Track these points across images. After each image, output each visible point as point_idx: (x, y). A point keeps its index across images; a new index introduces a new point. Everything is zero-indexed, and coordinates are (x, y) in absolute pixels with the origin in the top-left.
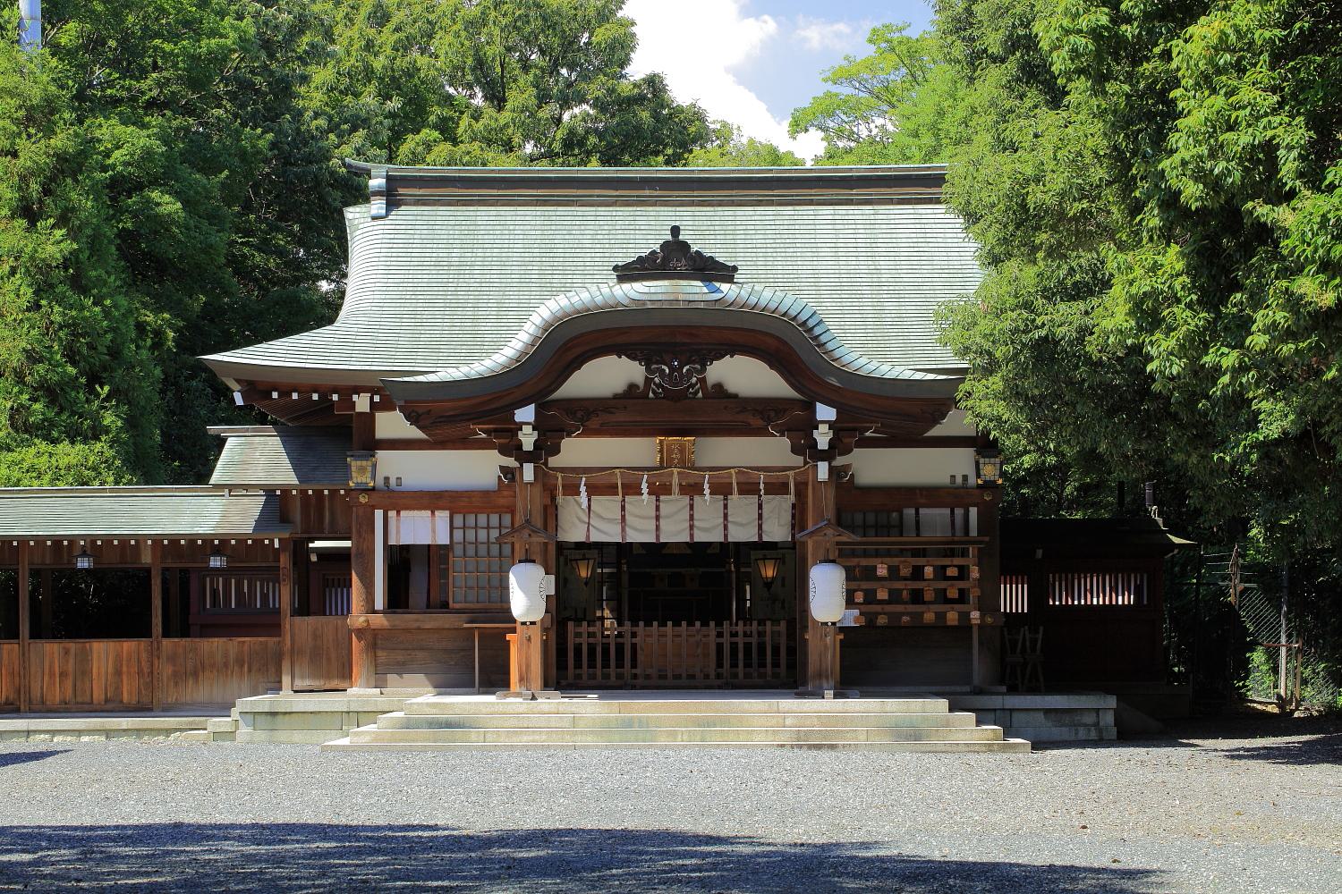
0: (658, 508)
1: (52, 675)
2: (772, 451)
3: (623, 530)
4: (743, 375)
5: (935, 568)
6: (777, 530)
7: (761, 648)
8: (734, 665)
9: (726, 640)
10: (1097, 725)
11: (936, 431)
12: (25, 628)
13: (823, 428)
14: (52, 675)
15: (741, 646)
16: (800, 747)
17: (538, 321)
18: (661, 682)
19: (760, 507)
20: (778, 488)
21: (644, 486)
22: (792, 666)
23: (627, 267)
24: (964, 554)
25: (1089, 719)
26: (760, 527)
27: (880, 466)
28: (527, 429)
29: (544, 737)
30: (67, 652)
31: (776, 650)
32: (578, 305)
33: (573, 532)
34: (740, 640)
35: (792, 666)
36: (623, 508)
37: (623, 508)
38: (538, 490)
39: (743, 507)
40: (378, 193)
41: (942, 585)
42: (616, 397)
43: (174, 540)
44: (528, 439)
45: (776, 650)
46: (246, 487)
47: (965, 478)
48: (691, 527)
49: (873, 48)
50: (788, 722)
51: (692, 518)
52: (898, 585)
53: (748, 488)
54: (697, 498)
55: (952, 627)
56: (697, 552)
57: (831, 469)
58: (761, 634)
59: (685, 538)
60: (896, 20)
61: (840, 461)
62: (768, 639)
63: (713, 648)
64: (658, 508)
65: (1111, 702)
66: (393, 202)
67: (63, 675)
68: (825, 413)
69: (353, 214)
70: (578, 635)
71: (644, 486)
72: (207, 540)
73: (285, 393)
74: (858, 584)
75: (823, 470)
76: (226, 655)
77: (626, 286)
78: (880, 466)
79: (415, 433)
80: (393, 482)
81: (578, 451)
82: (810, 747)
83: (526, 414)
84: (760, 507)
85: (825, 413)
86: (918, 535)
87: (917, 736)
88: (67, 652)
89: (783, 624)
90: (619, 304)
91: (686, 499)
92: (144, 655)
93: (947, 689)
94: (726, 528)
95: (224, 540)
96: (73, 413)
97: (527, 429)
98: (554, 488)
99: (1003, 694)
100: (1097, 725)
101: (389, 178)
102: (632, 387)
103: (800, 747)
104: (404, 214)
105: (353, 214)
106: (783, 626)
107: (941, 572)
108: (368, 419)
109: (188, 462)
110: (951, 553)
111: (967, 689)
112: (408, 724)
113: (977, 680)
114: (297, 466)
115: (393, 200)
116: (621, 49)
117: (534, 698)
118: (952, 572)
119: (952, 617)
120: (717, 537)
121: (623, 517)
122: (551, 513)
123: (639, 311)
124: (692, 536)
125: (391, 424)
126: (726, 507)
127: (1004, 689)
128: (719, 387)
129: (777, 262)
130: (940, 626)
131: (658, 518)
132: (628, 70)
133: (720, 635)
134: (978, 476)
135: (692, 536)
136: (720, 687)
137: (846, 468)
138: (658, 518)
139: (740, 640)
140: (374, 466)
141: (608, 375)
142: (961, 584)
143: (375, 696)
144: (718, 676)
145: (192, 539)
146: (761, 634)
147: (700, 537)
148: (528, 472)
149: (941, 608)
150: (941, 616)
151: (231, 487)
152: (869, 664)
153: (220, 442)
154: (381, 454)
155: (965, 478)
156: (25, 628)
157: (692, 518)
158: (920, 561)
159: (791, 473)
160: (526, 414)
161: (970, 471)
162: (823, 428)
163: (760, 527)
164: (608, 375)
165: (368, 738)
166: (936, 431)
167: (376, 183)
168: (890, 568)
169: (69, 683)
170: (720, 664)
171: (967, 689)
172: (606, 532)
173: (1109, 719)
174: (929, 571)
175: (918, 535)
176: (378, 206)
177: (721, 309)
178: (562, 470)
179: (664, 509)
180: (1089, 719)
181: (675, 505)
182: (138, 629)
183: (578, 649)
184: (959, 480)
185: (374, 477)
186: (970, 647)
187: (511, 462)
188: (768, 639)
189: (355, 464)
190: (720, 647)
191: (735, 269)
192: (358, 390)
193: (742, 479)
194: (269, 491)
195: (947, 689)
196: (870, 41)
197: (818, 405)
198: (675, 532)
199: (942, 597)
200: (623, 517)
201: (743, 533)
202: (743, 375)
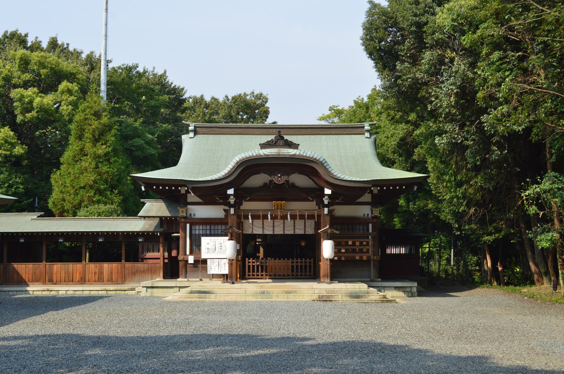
0: (274, 224)
1: (92, 274)
2: (310, 206)
3: (263, 230)
4: (300, 180)
5: (360, 242)
6: (310, 231)
7: (306, 266)
8: (297, 272)
9: (295, 264)
10: (411, 291)
11: (360, 200)
12: (123, 257)
13: (326, 197)
14: (92, 274)
15: (299, 267)
16: (320, 301)
17: (235, 162)
18: (253, 277)
19: (305, 223)
20: (311, 217)
21: (269, 216)
22: (315, 272)
23: (263, 144)
24: (368, 238)
25: (409, 290)
26: (305, 229)
27: (343, 211)
28: (232, 197)
29: (235, 297)
30: (96, 266)
31: (310, 266)
32: (248, 156)
33: (248, 231)
34: (299, 264)
35: (315, 272)
36: (263, 224)
37: (263, 224)
38: (235, 217)
39: (300, 223)
40: (192, 131)
41: (361, 247)
42: (260, 187)
43: (128, 233)
44: (232, 200)
45: (310, 266)
46: (149, 217)
47: (368, 215)
48: (284, 229)
49: (330, 112)
50: (316, 292)
51: (284, 227)
52: (348, 247)
53: (302, 217)
54: (286, 221)
55: (365, 261)
56: (284, 237)
57: (329, 211)
58: (306, 262)
59: (282, 233)
60: (336, 105)
61: (331, 208)
62: (308, 264)
63: (290, 267)
64: (274, 224)
65: (416, 284)
66: (196, 132)
67: (95, 273)
68: (328, 191)
69: (184, 137)
70: (249, 262)
71: (269, 216)
72: (138, 233)
73: (158, 187)
74: (337, 246)
75: (326, 210)
76: (144, 268)
77: (263, 150)
78: (343, 211)
79: (198, 200)
80: (192, 215)
81: (247, 205)
82: (323, 301)
83: (231, 191)
84: (305, 223)
85: (328, 191)
86: (159, 259)
87: (358, 297)
88: (96, 266)
89: (312, 259)
90: (261, 156)
91: (282, 221)
92: (119, 268)
93: (363, 280)
94: (294, 230)
95: (143, 233)
96: (106, 198)
97: (232, 197)
98: (241, 217)
99: (379, 281)
100: (411, 291)
101: (195, 127)
102: (265, 184)
103: (320, 301)
104: (199, 137)
105: (184, 137)
106: (312, 260)
107: (361, 244)
108: (185, 196)
109: (131, 210)
110: (363, 238)
111: (369, 280)
112: (192, 292)
113: (372, 277)
114: (170, 212)
115: (196, 132)
116: (266, 113)
117: (233, 283)
118: (364, 243)
119: (365, 258)
120: (291, 232)
121: (263, 226)
122: (240, 225)
123: (267, 158)
124: (284, 232)
125: (192, 197)
126: (294, 223)
127: (380, 280)
128: (293, 184)
129: (308, 147)
130: (361, 260)
131: (274, 227)
132: (268, 120)
133: (293, 262)
134: (372, 214)
135: (284, 232)
136: (292, 279)
137: (333, 210)
138: (274, 227)
139: (299, 264)
140: (187, 210)
141: (258, 180)
142: (367, 247)
143: (186, 281)
144: (293, 275)
145: (133, 232)
146: (306, 262)
147: (287, 232)
148: (232, 211)
149: (361, 254)
150: (361, 257)
151: (144, 217)
152: (340, 270)
153: (144, 204)
154: (189, 206)
155: (368, 215)
156: (123, 257)
157: (284, 227)
158: (347, 240)
159: (316, 212)
160: (231, 191)
161: (370, 213)
162: (326, 197)
163: (305, 229)
164: (258, 180)
165: (177, 297)
166: (360, 200)
167: (191, 128)
168: (353, 242)
169: (97, 276)
170: (293, 271)
171: (369, 280)
172: (258, 231)
173: (415, 290)
174: (358, 243)
175: (159, 259)
176: (191, 134)
177: (293, 158)
178: (244, 210)
179: (276, 224)
180: (409, 290)
181: (279, 223)
182: (117, 259)
183: (249, 266)
184: (366, 215)
185: (186, 213)
186: (370, 267)
187: (227, 208)
188: (308, 264)
189: (181, 210)
190: (293, 266)
191: (299, 145)
192: (181, 186)
193: (300, 213)
194: (161, 218)
195: (363, 280)
196: (329, 110)
197: (325, 189)
198: (279, 231)
199: (361, 251)
200: (263, 226)
201: (300, 231)
202: (300, 180)
